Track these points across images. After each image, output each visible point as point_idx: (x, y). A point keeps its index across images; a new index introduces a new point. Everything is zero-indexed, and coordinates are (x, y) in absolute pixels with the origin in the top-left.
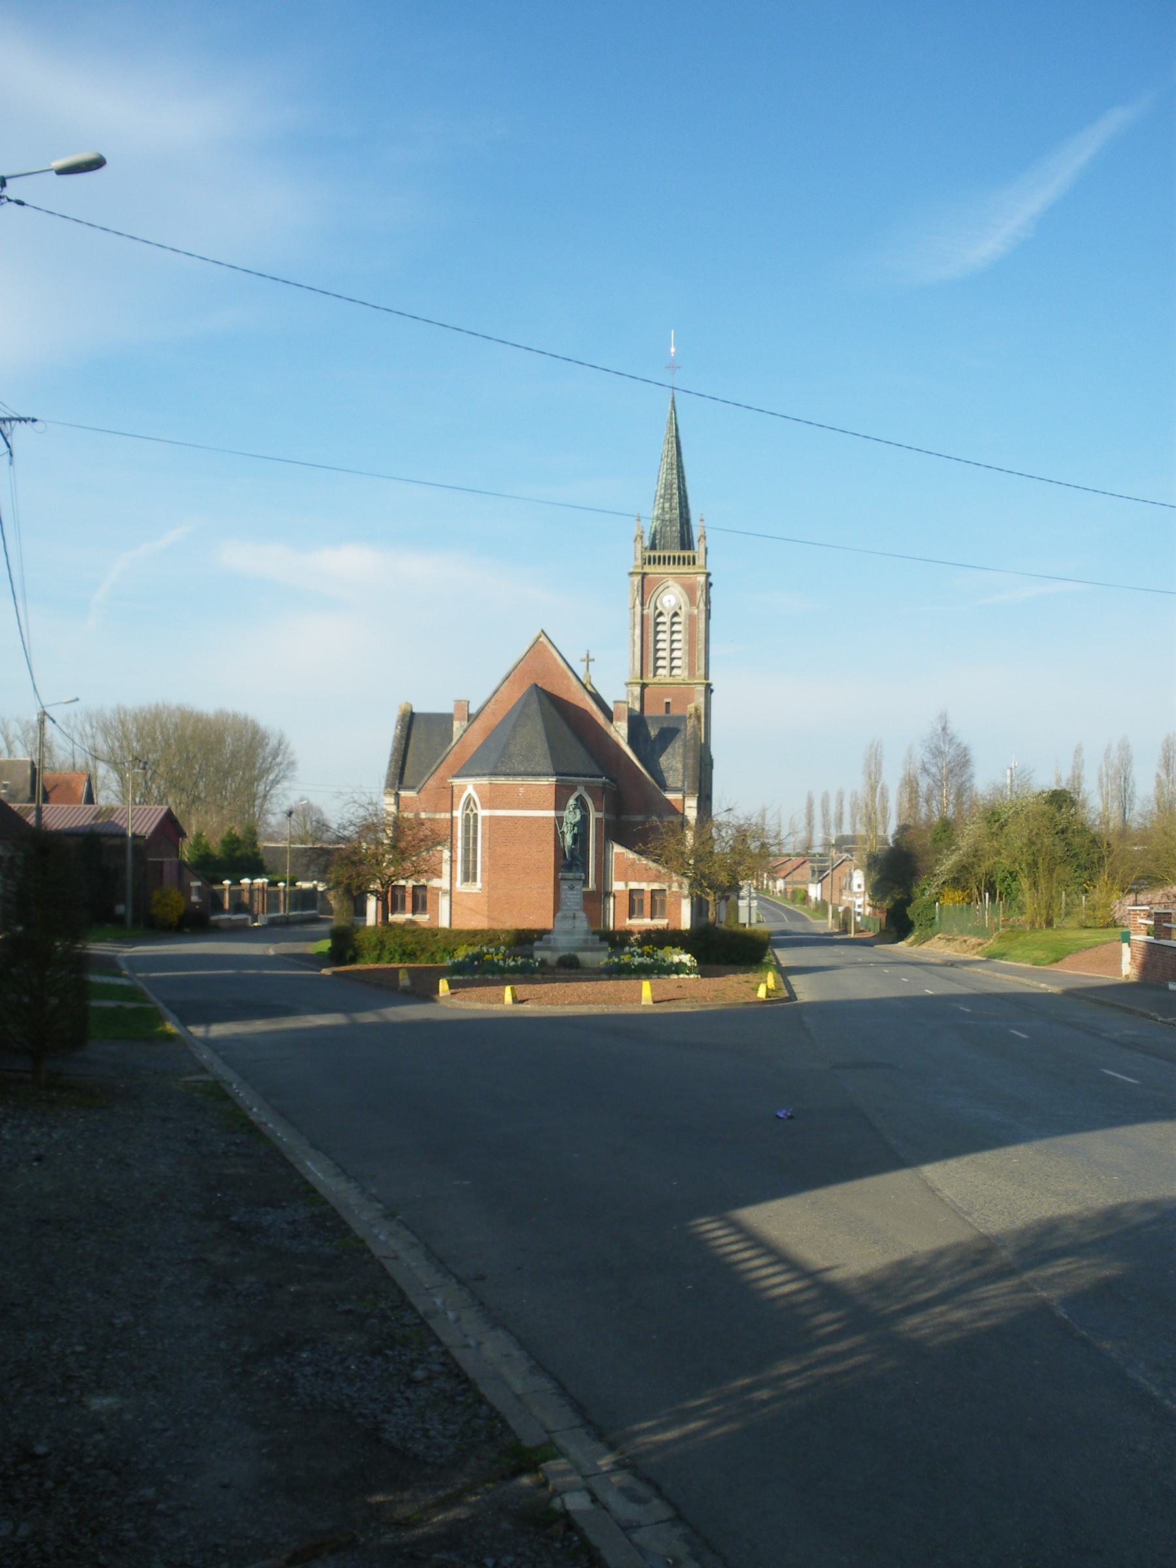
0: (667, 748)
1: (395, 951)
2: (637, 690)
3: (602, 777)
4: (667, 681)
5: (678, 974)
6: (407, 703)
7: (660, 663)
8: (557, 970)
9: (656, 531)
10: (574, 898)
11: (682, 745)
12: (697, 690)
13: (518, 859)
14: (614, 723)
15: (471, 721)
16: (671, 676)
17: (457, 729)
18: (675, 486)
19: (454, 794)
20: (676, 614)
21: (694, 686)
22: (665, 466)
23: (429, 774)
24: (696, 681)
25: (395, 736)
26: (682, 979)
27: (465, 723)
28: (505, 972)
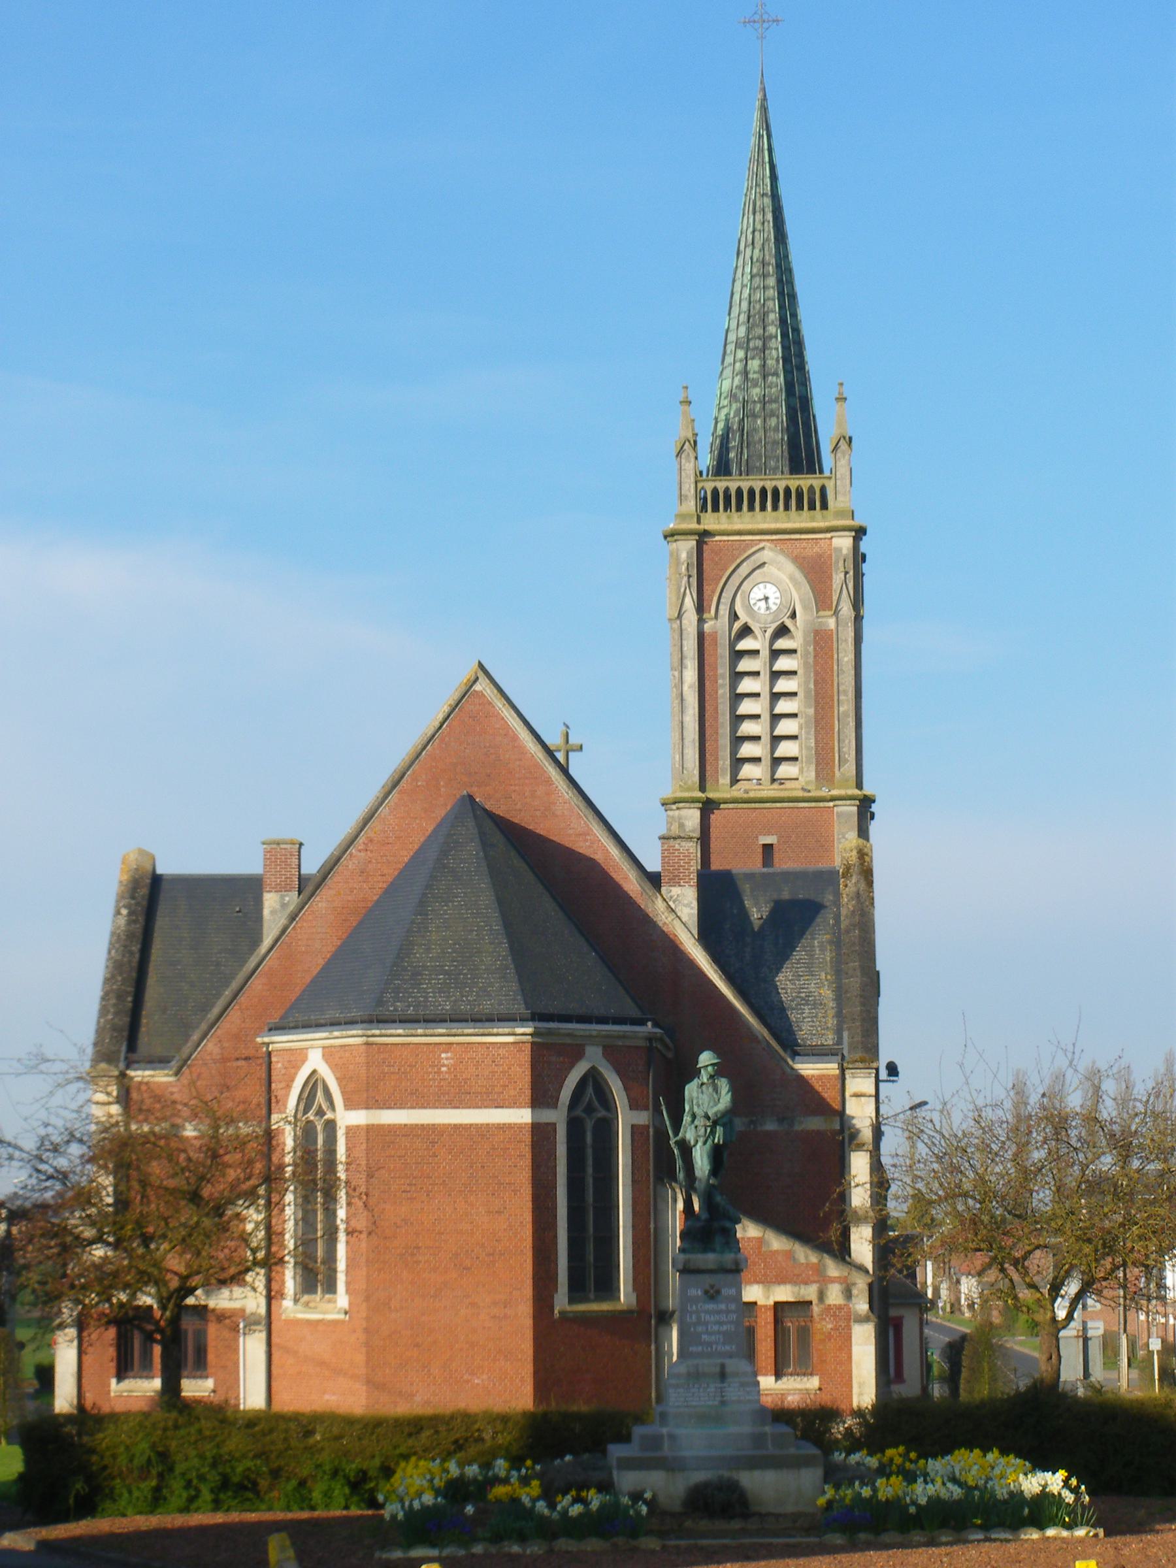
0: (793, 949)
1: (202, 1478)
2: (692, 817)
3: (641, 1022)
4: (765, 794)
5: (1041, 1527)
6: (142, 852)
7: (747, 750)
8: (688, 1523)
9: (728, 429)
10: (720, 1323)
11: (830, 942)
12: (839, 815)
13: (440, 1233)
14: (663, 890)
15: (306, 893)
16: (773, 780)
17: (273, 912)
18: (773, 317)
19: (274, 1073)
20: (782, 631)
21: (831, 804)
22: (748, 270)
23: (204, 1026)
24: (835, 792)
25: (113, 934)
26: (1055, 1538)
27: (292, 898)
28: (555, 1536)
